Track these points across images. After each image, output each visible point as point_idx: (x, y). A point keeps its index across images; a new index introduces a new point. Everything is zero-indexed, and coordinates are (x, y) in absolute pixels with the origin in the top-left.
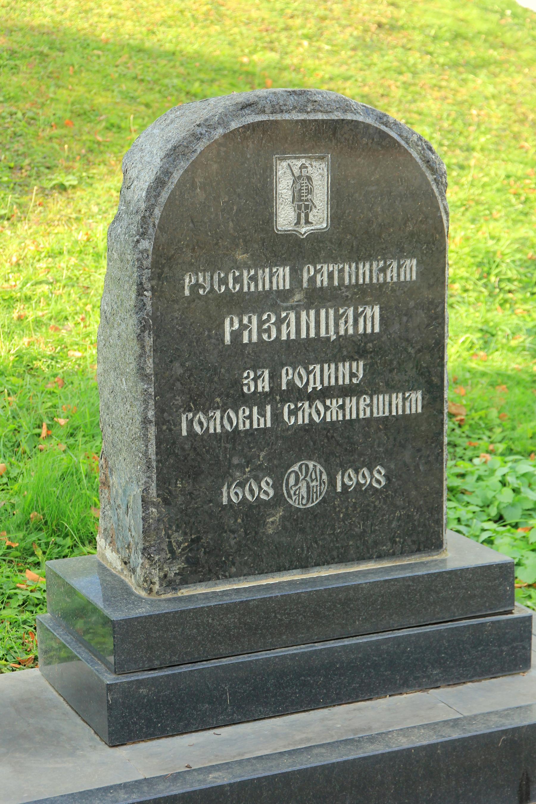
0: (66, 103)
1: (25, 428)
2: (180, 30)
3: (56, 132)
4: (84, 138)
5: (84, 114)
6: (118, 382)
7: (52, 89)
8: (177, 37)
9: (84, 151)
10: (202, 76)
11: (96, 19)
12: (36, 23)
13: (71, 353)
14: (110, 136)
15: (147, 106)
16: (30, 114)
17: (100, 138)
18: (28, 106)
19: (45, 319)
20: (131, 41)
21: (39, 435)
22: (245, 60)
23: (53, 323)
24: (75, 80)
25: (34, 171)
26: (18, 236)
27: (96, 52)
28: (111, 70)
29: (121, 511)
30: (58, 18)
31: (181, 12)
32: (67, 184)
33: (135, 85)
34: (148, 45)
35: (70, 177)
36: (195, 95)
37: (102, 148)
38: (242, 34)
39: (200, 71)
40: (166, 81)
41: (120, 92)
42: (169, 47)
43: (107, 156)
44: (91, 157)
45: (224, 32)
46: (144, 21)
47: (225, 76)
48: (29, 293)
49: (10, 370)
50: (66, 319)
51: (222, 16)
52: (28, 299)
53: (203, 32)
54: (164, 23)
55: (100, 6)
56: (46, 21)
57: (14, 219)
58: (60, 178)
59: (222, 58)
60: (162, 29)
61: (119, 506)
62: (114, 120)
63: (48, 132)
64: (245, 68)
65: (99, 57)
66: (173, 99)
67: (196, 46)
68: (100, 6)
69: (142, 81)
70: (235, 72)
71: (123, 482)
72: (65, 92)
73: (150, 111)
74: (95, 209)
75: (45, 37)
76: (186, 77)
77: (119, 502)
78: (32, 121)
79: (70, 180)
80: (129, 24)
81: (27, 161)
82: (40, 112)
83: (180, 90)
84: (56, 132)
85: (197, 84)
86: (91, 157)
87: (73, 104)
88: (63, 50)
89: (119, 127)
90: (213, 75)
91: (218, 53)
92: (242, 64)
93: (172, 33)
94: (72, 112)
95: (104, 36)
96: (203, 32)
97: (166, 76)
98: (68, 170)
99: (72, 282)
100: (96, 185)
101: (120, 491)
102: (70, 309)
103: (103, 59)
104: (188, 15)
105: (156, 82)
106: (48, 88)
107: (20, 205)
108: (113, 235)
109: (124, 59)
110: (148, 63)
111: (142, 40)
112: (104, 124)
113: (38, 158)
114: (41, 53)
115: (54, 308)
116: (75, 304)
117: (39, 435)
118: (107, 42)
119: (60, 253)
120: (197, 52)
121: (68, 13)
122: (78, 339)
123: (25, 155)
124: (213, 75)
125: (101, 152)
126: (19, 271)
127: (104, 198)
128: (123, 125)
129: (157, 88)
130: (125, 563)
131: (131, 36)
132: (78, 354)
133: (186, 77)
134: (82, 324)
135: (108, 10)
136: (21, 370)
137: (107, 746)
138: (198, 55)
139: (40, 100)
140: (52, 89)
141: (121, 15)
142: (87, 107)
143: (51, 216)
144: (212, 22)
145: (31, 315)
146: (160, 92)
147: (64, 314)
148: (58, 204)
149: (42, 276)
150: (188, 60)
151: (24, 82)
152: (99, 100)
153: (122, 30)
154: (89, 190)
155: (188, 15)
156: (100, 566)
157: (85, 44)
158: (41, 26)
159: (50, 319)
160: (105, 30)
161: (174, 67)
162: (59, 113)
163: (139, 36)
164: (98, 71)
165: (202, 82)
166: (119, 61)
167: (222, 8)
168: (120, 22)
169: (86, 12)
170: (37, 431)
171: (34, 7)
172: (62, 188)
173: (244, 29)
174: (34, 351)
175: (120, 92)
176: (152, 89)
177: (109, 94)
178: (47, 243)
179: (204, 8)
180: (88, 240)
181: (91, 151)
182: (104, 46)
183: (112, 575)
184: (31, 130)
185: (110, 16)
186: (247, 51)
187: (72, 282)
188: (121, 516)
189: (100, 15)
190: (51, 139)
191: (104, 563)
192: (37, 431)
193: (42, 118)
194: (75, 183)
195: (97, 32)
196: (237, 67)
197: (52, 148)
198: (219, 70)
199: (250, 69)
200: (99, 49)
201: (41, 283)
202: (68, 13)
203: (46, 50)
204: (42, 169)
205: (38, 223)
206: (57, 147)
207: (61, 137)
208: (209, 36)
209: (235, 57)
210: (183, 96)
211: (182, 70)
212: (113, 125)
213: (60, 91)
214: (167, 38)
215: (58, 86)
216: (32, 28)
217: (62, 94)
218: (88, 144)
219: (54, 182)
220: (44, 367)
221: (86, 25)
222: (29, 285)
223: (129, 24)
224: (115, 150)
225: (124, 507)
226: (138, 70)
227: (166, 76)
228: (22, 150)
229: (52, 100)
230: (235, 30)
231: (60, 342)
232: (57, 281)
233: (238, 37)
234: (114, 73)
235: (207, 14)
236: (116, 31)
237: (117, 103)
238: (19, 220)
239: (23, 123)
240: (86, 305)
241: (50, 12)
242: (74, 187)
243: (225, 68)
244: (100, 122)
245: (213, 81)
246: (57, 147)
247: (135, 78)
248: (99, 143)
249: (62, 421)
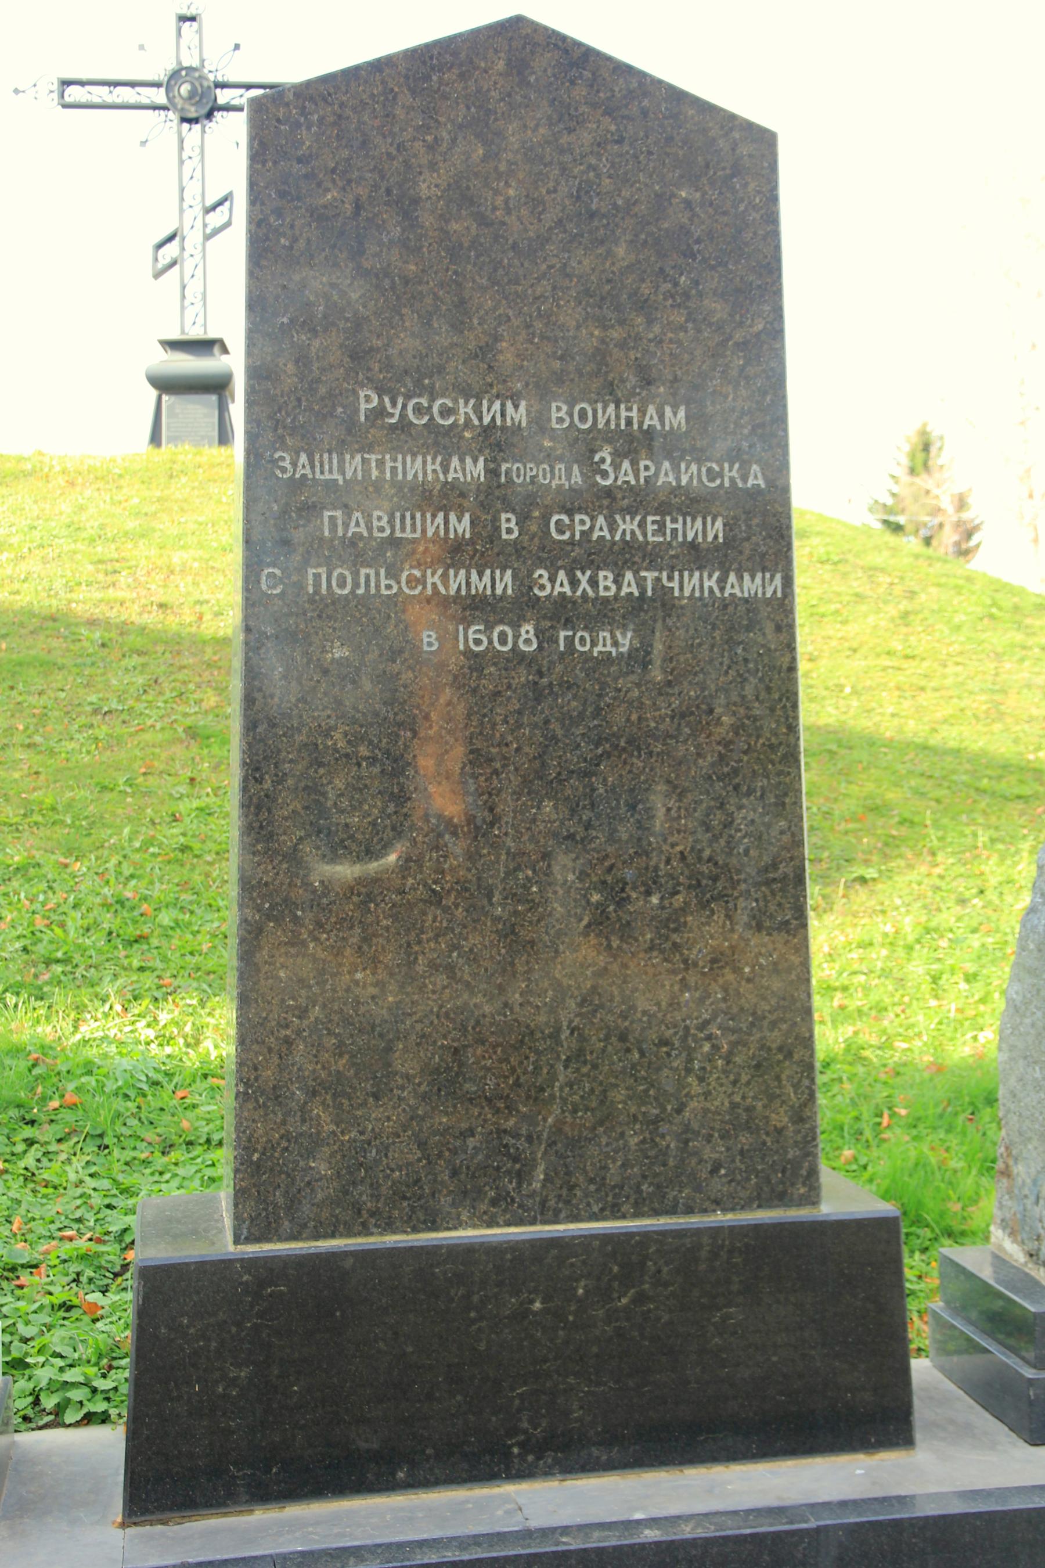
0: (858, 799)
1: (865, 1116)
2: (962, 728)
3: (852, 826)
4: (879, 832)
5: (877, 809)
6: (1030, 1070)
7: (843, 785)
8: (960, 734)
9: (879, 845)
10: (989, 772)
11: (878, 718)
12: (821, 722)
13: (897, 1044)
14: (904, 831)
15: (938, 801)
16: (824, 809)
17: (894, 833)
18: (822, 801)
19: (865, 1009)
20: (916, 740)
21: (879, 1124)
22: (1031, 757)
23: (873, 1013)
24: (863, 776)
25: (834, 864)
26: (826, 926)
27: (883, 750)
28: (900, 766)
29: (1029, 1202)
30: (843, 718)
31: (962, 710)
32: (868, 876)
33: (923, 781)
34: (932, 742)
35: (871, 870)
36: (984, 791)
37: (897, 842)
38: (1024, 732)
39: (987, 767)
40: (954, 777)
41: (910, 788)
42: (952, 744)
43: (903, 849)
44: (888, 851)
45: (1007, 730)
46: (926, 719)
47: (1012, 773)
48: (846, 982)
49: (841, 1058)
50: (886, 1009)
51: (1002, 715)
52: (845, 989)
53: (985, 729)
54: (945, 721)
55: (881, 706)
56: (831, 721)
57: (820, 910)
58: (860, 871)
59: (1007, 756)
60: (945, 727)
61: (1026, 1196)
62: (907, 815)
63: (843, 826)
64: (1031, 765)
65: (886, 754)
66: (963, 795)
67: (981, 744)
68: (881, 706)
69: (930, 777)
70: (1022, 769)
71: (1033, 1171)
72: (857, 788)
73: (941, 807)
74: (898, 902)
75: (832, 736)
76: (973, 773)
77: (1026, 1191)
78: (827, 815)
79: (870, 873)
80: (912, 723)
81: (826, 854)
82: (835, 806)
83: (968, 786)
84: (852, 826)
85: (985, 781)
86: (888, 851)
87: (865, 799)
88: (850, 748)
89: (912, 822)
90: (1000, 772)
91: (1003, 750)
92: (1029, 761)
93: (954, 732)
94: (864, 806)
95: (888, 734)
96: (985, 729)
97: (954, 772)
98: (867, 862)
99: (885, 973)
100: (896, 878)
101: (1028, 1181)
102: (887, 1000)
103: (890, 757)
104: (969, 713)
105: (944, 778)
106: (839, 783)
107: (824, 897)
108: (1029, 926)
109: (912, 756)
110: (936, 759)
111: (926, 738)
112: (897, 819)
113: (837, 851)
114: (830, 751)
115: (874, 997)
116: (893, 996)
117: (879, 1124)
118: (891, 740)
119: (871, 944)
120: (982, 750)
121: (852, 712)
122: (901, 1030)
123: (822, 848)
124: (1000, 772)
125: (898, 846)
126: (833, 961)
127: (907, 891)
128: (916, 819)
129: (946, 784)
130: (1031, 1255)
131: (915, 734)
132: (904, 1045)
133: (973, 773)
134: (903, 1016)
135: (890, 710)
136: (850, 1058)
137: (1026, 1445)
138: (983, 753)
139: (832, 796)
140: (843, 785)
141: (903, 714)
142: (878, 802)
143: (855, 908)
144: (993, 721)
145: (853, 1004)
146: (949, 788)
147: (882, 1005)
148: (861, 894)
149: (856, 967)
150: (974, 758)
151: (815, 779)
152: (890, 796)
153: (906, 729)
154: (890, 883)
155: (969, 713)
156: (996, 1257)
157: (871, 742)
158: (826, 725)
159: (871, 1009)
160: (888, 730)
161: (960, 764)
162: (853, 808)
163: (922, 734)
164: (886, 768)
165: (990, 778)
166: (906, 758)
167: (1002, 707)
168: (902, 721)
169: (868, 711)
170: (878, 1120)
171: (818, 708)
172: (863, 880)
173: (1026, 727)
174: (862, 1039)
175: (910, 788)
176: (940, 785)
177: (898, 789)
178: (856, 934)
179: (984, 707)
180: (897, 932)
181: (886, 844)
182: (889, 743)
183: (1014, 1267)
184: (827, 824)
185: (893, 715)
186: (1031, 748)
187: (885, 973)
188: (1029, 1207)
189: (882, 714)
190: (846, 833)
191: (1001, 1255)
192: (878, 1120)
193: (837, 812)
194: (876, 875)
195: (882, 731)
196: (1023, 764)
197: (849, 842)
198: (1005, 767)
199: (1037, 765)
200: (885, 746)
201: (855, 973)
202: (852, 712)
203: (834, 747)
204: (842, 862)
205: (844, 914)
206: (854, 841)
207: (855, 832)
208: (993, 734)
209: (1020, 754)
210: (972, 792)
211: (968, 766)
212: (905, 820)
213: (853, 786)
214: (950, 736)
215: (849, 782)
216: (819, 728)
217: (854, 789)
218: (883, 838)
219: (855, 875)
220: (872, 1056)
221: (870, 724)
222: (845, 975)
223: (912, 723)
224: (911, 843)
225: (1032, 1198)
226: (925, 766)
227: (954, 772)
228: (820, 843)
229: (845, 795)
230: (1018, 728)
231: (884, 1031)
232: (871, 972)
233: (1021, 735)
234: (902, 769)
235: (987, 712)
236: (900, 730)
237: (907, 799)
238: (825, 911)
239: (819, 818)
240: (903, 996)
241: (833, 712)
242: (874, 880)
243: (1011, 765)
244: (893, 816)
245: (1000, 778)
246: (854, 841)
247: (922, 775)
248: (894, 837)
249: (903, 1112)
